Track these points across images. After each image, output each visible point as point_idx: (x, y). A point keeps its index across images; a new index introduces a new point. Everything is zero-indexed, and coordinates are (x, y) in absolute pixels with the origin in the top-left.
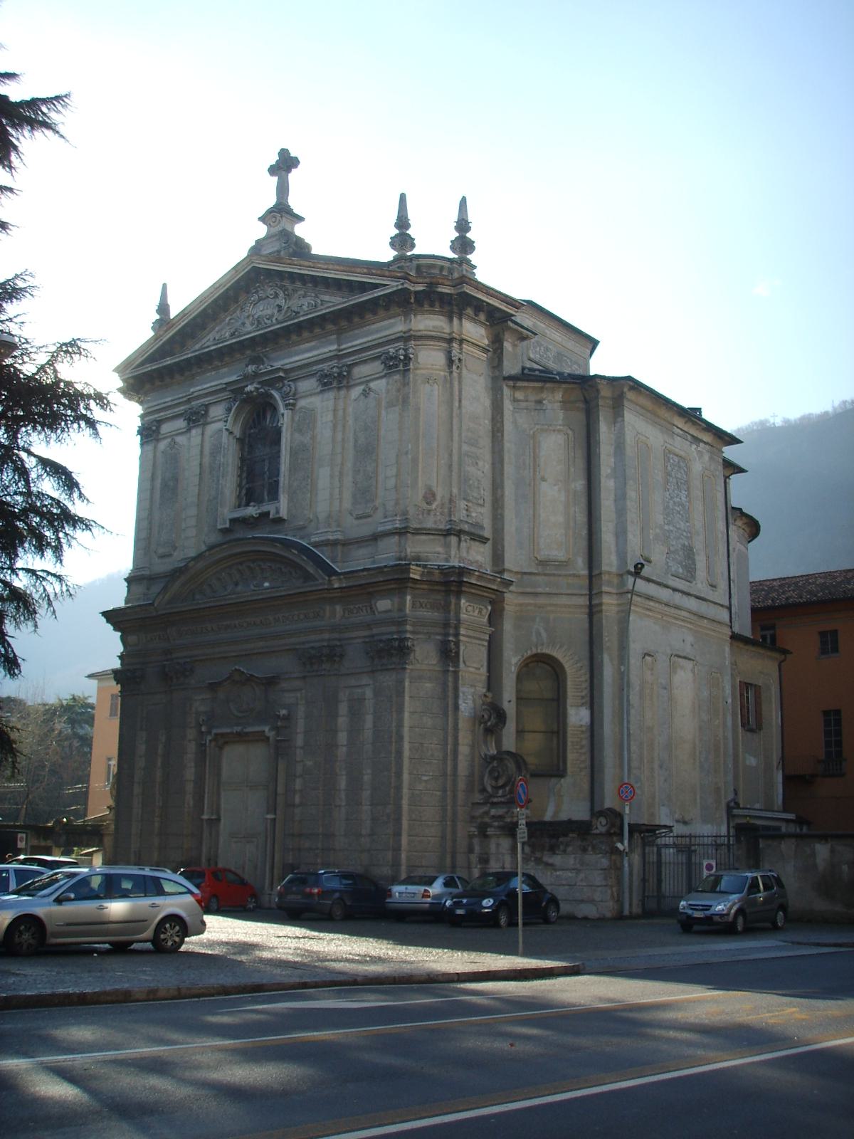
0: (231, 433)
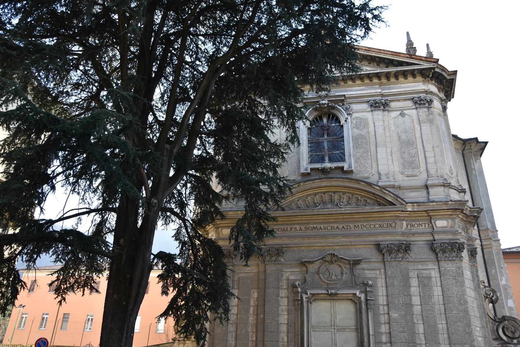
0: (304, 124)
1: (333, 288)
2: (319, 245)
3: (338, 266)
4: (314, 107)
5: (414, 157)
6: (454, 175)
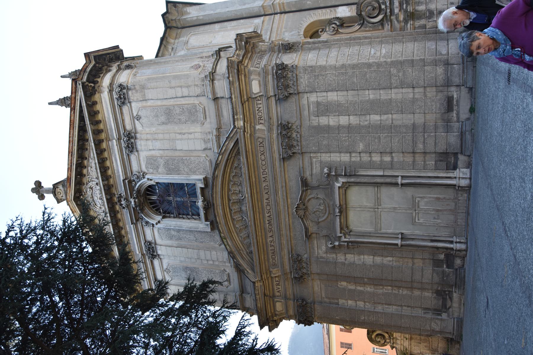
0: (159, 222)
1: (334, 210)
2: (287, 220)
3: (310, 202)
4: (139, 212)
5: (183, 109)
6: (201, 64)
